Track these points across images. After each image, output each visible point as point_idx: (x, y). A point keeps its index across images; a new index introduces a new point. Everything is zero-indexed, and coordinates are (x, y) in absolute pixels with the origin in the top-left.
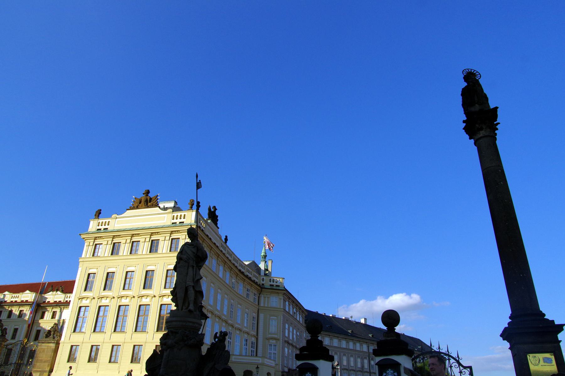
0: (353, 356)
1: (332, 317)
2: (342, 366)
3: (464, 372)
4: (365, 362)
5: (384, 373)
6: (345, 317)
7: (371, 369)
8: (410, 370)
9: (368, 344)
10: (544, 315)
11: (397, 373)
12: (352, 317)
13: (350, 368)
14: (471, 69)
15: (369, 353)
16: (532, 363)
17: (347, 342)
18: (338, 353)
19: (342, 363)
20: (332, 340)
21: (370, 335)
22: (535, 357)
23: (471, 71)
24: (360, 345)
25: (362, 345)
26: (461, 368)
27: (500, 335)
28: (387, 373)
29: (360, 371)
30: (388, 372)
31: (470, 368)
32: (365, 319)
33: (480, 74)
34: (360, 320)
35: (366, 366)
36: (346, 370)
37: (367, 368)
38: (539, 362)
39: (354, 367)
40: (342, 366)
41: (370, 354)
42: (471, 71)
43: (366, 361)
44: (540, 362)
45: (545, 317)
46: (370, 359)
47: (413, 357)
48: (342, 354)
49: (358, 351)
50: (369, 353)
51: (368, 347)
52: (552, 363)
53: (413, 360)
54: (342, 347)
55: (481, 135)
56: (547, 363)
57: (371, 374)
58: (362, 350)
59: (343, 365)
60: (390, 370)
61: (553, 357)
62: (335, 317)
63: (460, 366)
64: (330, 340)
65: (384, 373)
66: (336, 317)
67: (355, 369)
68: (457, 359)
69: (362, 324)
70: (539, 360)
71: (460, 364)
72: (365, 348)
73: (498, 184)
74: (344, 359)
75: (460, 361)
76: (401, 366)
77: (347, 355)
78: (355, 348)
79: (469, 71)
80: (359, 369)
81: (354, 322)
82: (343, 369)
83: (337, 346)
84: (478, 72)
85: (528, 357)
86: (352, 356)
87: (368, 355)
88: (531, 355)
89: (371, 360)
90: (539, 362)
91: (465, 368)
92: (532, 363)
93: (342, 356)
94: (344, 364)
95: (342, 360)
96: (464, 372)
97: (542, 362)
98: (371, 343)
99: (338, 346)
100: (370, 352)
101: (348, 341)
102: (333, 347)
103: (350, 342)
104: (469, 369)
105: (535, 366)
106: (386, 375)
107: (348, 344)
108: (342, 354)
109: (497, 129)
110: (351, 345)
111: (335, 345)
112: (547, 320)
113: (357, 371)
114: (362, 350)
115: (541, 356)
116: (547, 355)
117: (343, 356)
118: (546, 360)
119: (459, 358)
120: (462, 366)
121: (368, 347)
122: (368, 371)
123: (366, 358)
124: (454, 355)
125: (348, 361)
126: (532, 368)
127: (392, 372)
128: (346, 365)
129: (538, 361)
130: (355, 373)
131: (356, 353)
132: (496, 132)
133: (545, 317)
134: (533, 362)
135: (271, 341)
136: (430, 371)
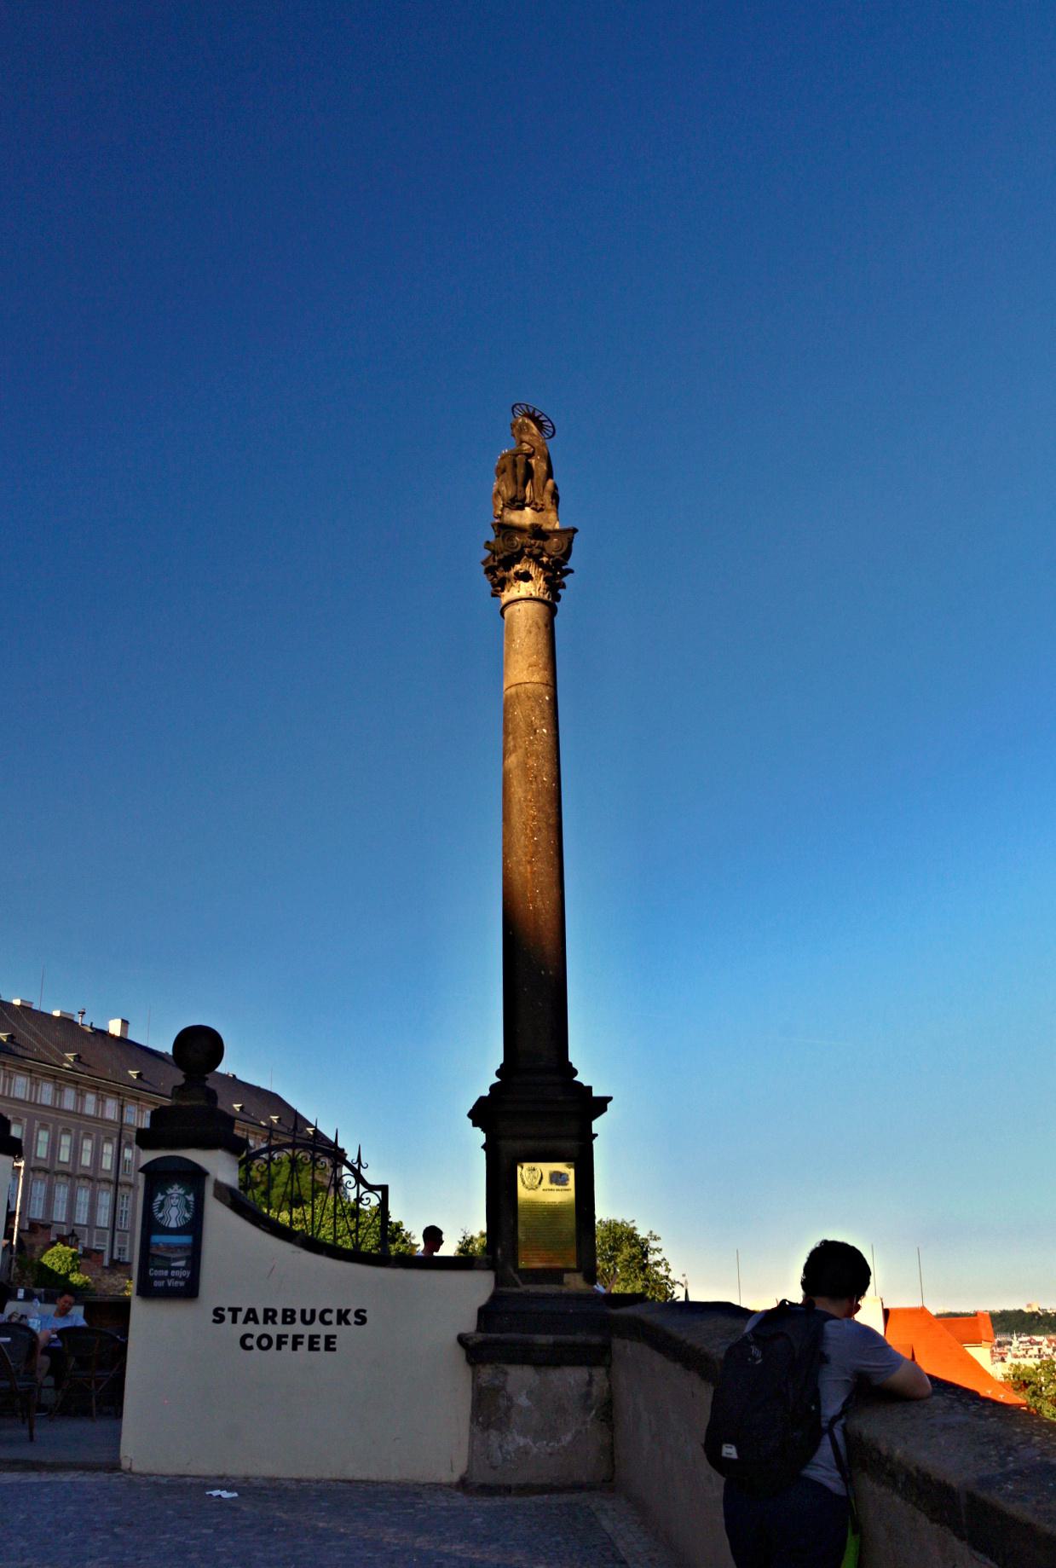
0: (70, 1131)
1: (21, 1006)
2: (33, 1158)
3: (367, 1199)
4: (84, 1147)
5: (159, 1195)
6: (61, 1012)
7: (120, 1173)
8: (230, 1190)
9: (121, 1097)
10: (575, 1072)
11: (194, 1196)
12: (83, 1013)
13: (58, 1167)
14: (535, 409)
15: (122, 1124)
16: (524, 1183)
17: (79, 1092)
18: (26, 1120)
19: (33, 1150)
20: (11, 1078)
21: (133, 1073)
22: (534, 1170)
23: (534, 412)
24: (98, 1100)
25: (104, 1101)
26: (362, 1189)
27: (470, 1105)
28: (166, 1194)
29: (85, 1177)
30: (170, 1191)
31: (384, 1189)
32: (125, 1023)
33: (553, 427)
34: (108, 1025)
35: (107, 1163)
36: (65, 1177)
37: (108, 1167)
38: (540, 1183)
39: (71, 1165)
40: (33, 1158)
41: (126, 1127)
42: (534, 412)
43: (108, 1149)
44: (543, 1180)
45: (576, 1079)
46: (123, 1142)
47: (244, 1155)
48: (37, 1124)
49: (88, 1116)
50: (122, 1124)
51: (122, 1107)
52: (566, 1185)
53: (241, 1164)
54: (38, 1102)
55: (523, 594)
56: (557, 1184)
57: (119, 1189)
58: (60, 1105)
59: (36, 1157)
60: (176, 1187)
61: (571, 1173)
62: (30, 1009)
63: (361, 1185)
64: (32, 1084)
65: (159, 1195)
66: (34, 1008)
67: (70, 1170)
68: (356, 1166)
69: (113, 1036)
70: (542, 1178)
71: (360, 1180)
72: (111, 1110)
73: (535, 731)
74: (40, 1138)
75: (363, 1172)
76: (207, 1178)
77: (51, 1126)
78: (82, 1108)
79: (528, 410)
80: (83, 1172)
81: (90, 1030)
82: (33, 1170)
83: (23, 1097)
84: (549, 420)
85: (519, 1169)
86: (67, 1131)
87: (118, 1130)
88: (527, 1165)
89: (125, 1147)
90: (540, 1183)
91: (371, 1188)
92: (524, 1183)
93: (35, 1130)
94: (38, 1155)
95: (34, 1142)
96: (367, 1199)
97: (546, 1183)
98: (133, 1097)
99: (27, 1099)
100: (124, 1121)
101: (60, 1084)
102: (38, 1105)
103: (66, 1089)
104: (379, 1193)
105: (530, 1189)
106: (164, 1200)
107: (10, 1082)
108: (37, 1124)
109: (564, 586)
110: (69, 1100)
111: (17, 1096)
112: (580, 1084)
113: (78, 1177)
114: (100, 1116)
115: (547, 1168)
116: (560, 1167)
117: (38, 1130)
118: (557, 1178)
119: (360, 1164)
120: (366, 1184)
121: (122, 1107)
122: (112, 1177)
123: (109, 1140)
124: (351, 1157)
125: (54, 1147)
126: (523, 1193)
127: (181, 1191)
128: (44, 1156)
129: (538, 1181)
130: (91, 1184)
131: (82, 1122)
132: (561, 591)
133: (576, 1079)
134: (526, 1183)
135: (324, 1219)
136: (134, 1143)
